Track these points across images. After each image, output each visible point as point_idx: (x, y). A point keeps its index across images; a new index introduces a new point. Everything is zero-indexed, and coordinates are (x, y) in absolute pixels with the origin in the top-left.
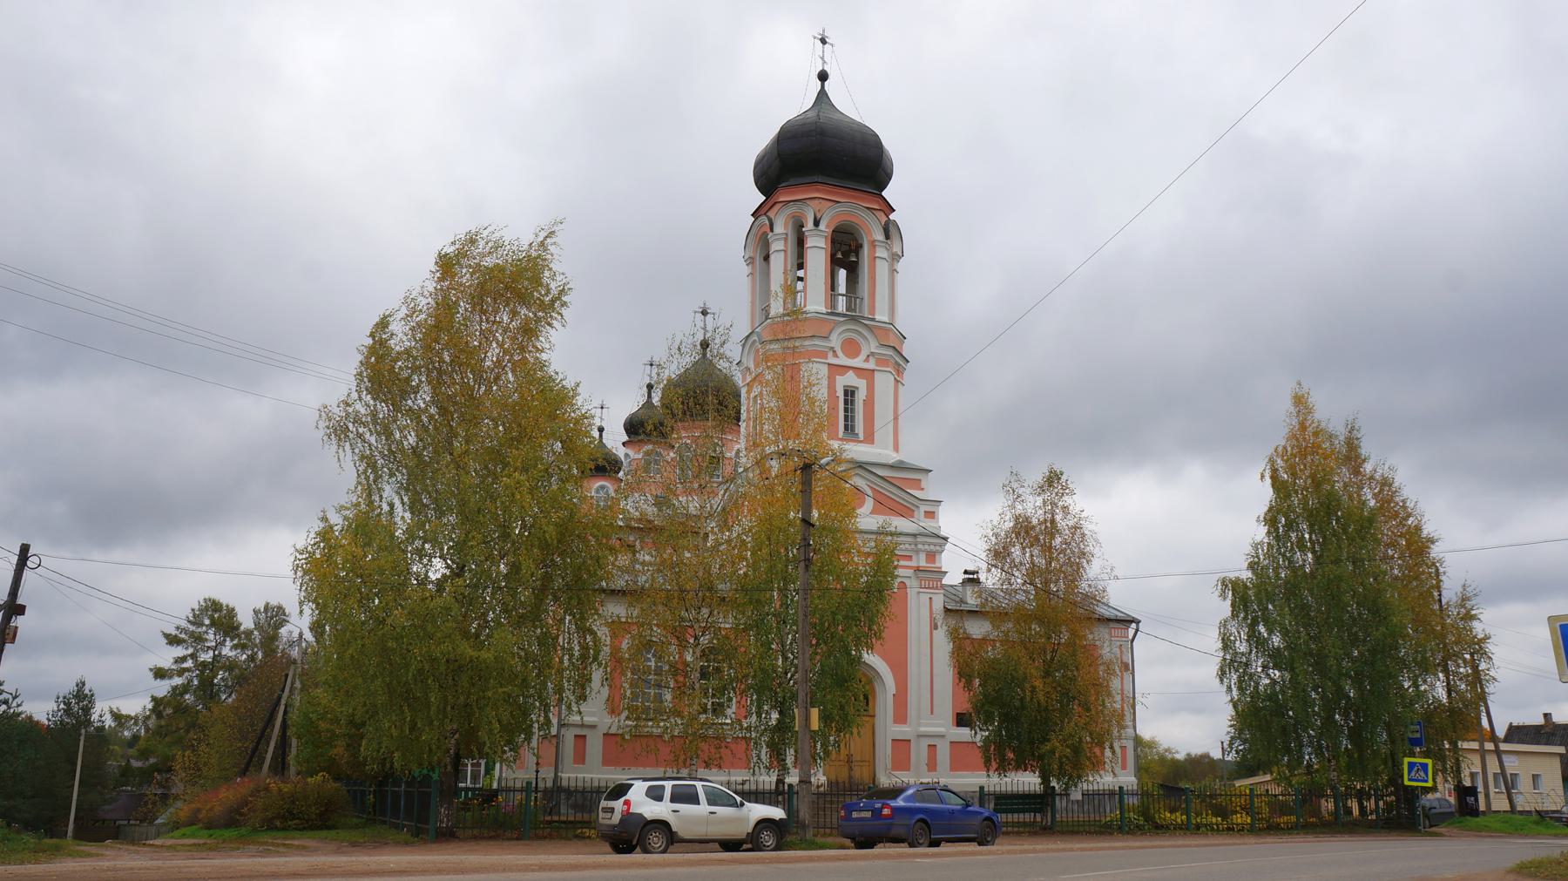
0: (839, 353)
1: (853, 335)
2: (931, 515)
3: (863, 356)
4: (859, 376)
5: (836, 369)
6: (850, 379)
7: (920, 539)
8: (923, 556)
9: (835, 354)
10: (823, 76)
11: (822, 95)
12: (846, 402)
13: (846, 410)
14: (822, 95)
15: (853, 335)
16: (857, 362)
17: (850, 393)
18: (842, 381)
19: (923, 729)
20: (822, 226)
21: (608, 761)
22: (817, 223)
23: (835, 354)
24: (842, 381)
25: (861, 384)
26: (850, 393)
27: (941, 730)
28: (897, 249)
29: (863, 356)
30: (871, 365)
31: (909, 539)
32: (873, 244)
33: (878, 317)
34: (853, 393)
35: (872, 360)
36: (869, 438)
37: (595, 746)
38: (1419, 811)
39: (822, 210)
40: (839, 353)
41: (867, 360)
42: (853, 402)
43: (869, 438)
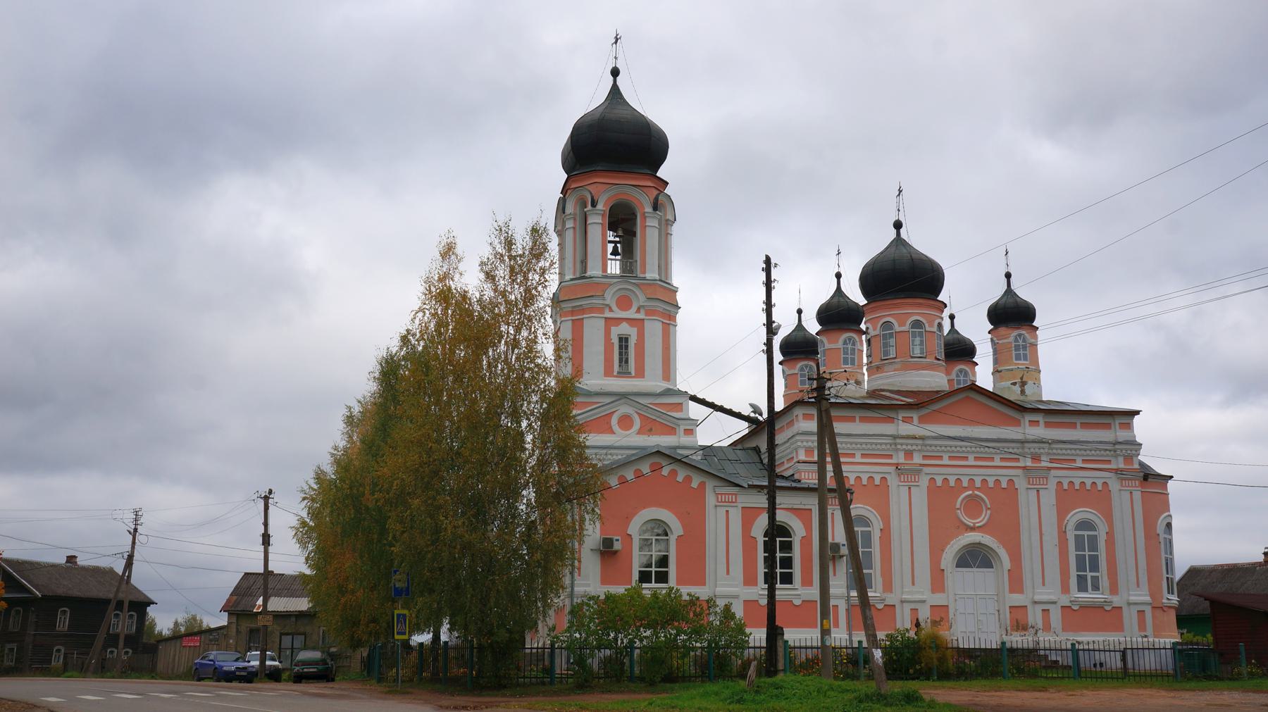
0: (614, 307)
1: (628, 293)
2: (690, 432)
3: (634, 308)
4: (631, 326)
5: (610, 322)
6: (624, 329)
7: (898, 441)
8: (902, 455)
9: (611, 310)
10: (615, 73)
11: (615, 92)
12: (621, 347)
13: (620, 354)
14: (615, 92)
15: (628, 293)
16: (630, 314)
17: (624, 341)
18: (616, 331)
19: (905, 597)
20: (600, 206)
21: (1065, 628)
22: (594, 204)
23: (611, 310)
24: (616, 331)
25: (632, 332)
26: (624, 341)
27: (1053, 598)
28: (670, 217)
29: (634, 308)
30: (641, 316)
31: (920, 442)
32: (644, 218)
33: (648, 276)
34: (627, 339)
35: (642, 311)
36: (640, 373)
37: (1056, 617)
38: (780, 643)
39: (606, 190)
40: (614, 307)
41: (638, 311)
42: (627, 347)
43: (640, 373)
